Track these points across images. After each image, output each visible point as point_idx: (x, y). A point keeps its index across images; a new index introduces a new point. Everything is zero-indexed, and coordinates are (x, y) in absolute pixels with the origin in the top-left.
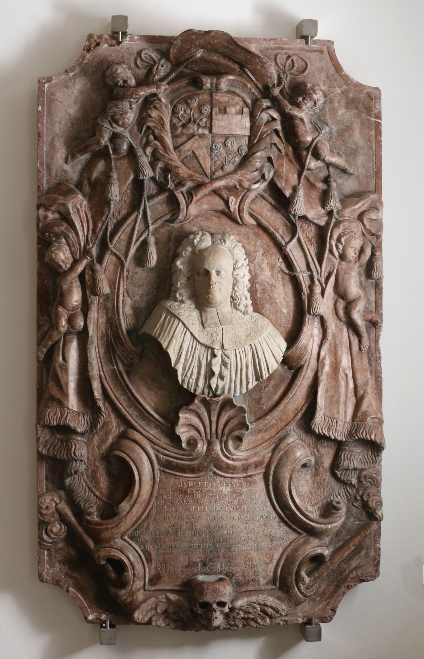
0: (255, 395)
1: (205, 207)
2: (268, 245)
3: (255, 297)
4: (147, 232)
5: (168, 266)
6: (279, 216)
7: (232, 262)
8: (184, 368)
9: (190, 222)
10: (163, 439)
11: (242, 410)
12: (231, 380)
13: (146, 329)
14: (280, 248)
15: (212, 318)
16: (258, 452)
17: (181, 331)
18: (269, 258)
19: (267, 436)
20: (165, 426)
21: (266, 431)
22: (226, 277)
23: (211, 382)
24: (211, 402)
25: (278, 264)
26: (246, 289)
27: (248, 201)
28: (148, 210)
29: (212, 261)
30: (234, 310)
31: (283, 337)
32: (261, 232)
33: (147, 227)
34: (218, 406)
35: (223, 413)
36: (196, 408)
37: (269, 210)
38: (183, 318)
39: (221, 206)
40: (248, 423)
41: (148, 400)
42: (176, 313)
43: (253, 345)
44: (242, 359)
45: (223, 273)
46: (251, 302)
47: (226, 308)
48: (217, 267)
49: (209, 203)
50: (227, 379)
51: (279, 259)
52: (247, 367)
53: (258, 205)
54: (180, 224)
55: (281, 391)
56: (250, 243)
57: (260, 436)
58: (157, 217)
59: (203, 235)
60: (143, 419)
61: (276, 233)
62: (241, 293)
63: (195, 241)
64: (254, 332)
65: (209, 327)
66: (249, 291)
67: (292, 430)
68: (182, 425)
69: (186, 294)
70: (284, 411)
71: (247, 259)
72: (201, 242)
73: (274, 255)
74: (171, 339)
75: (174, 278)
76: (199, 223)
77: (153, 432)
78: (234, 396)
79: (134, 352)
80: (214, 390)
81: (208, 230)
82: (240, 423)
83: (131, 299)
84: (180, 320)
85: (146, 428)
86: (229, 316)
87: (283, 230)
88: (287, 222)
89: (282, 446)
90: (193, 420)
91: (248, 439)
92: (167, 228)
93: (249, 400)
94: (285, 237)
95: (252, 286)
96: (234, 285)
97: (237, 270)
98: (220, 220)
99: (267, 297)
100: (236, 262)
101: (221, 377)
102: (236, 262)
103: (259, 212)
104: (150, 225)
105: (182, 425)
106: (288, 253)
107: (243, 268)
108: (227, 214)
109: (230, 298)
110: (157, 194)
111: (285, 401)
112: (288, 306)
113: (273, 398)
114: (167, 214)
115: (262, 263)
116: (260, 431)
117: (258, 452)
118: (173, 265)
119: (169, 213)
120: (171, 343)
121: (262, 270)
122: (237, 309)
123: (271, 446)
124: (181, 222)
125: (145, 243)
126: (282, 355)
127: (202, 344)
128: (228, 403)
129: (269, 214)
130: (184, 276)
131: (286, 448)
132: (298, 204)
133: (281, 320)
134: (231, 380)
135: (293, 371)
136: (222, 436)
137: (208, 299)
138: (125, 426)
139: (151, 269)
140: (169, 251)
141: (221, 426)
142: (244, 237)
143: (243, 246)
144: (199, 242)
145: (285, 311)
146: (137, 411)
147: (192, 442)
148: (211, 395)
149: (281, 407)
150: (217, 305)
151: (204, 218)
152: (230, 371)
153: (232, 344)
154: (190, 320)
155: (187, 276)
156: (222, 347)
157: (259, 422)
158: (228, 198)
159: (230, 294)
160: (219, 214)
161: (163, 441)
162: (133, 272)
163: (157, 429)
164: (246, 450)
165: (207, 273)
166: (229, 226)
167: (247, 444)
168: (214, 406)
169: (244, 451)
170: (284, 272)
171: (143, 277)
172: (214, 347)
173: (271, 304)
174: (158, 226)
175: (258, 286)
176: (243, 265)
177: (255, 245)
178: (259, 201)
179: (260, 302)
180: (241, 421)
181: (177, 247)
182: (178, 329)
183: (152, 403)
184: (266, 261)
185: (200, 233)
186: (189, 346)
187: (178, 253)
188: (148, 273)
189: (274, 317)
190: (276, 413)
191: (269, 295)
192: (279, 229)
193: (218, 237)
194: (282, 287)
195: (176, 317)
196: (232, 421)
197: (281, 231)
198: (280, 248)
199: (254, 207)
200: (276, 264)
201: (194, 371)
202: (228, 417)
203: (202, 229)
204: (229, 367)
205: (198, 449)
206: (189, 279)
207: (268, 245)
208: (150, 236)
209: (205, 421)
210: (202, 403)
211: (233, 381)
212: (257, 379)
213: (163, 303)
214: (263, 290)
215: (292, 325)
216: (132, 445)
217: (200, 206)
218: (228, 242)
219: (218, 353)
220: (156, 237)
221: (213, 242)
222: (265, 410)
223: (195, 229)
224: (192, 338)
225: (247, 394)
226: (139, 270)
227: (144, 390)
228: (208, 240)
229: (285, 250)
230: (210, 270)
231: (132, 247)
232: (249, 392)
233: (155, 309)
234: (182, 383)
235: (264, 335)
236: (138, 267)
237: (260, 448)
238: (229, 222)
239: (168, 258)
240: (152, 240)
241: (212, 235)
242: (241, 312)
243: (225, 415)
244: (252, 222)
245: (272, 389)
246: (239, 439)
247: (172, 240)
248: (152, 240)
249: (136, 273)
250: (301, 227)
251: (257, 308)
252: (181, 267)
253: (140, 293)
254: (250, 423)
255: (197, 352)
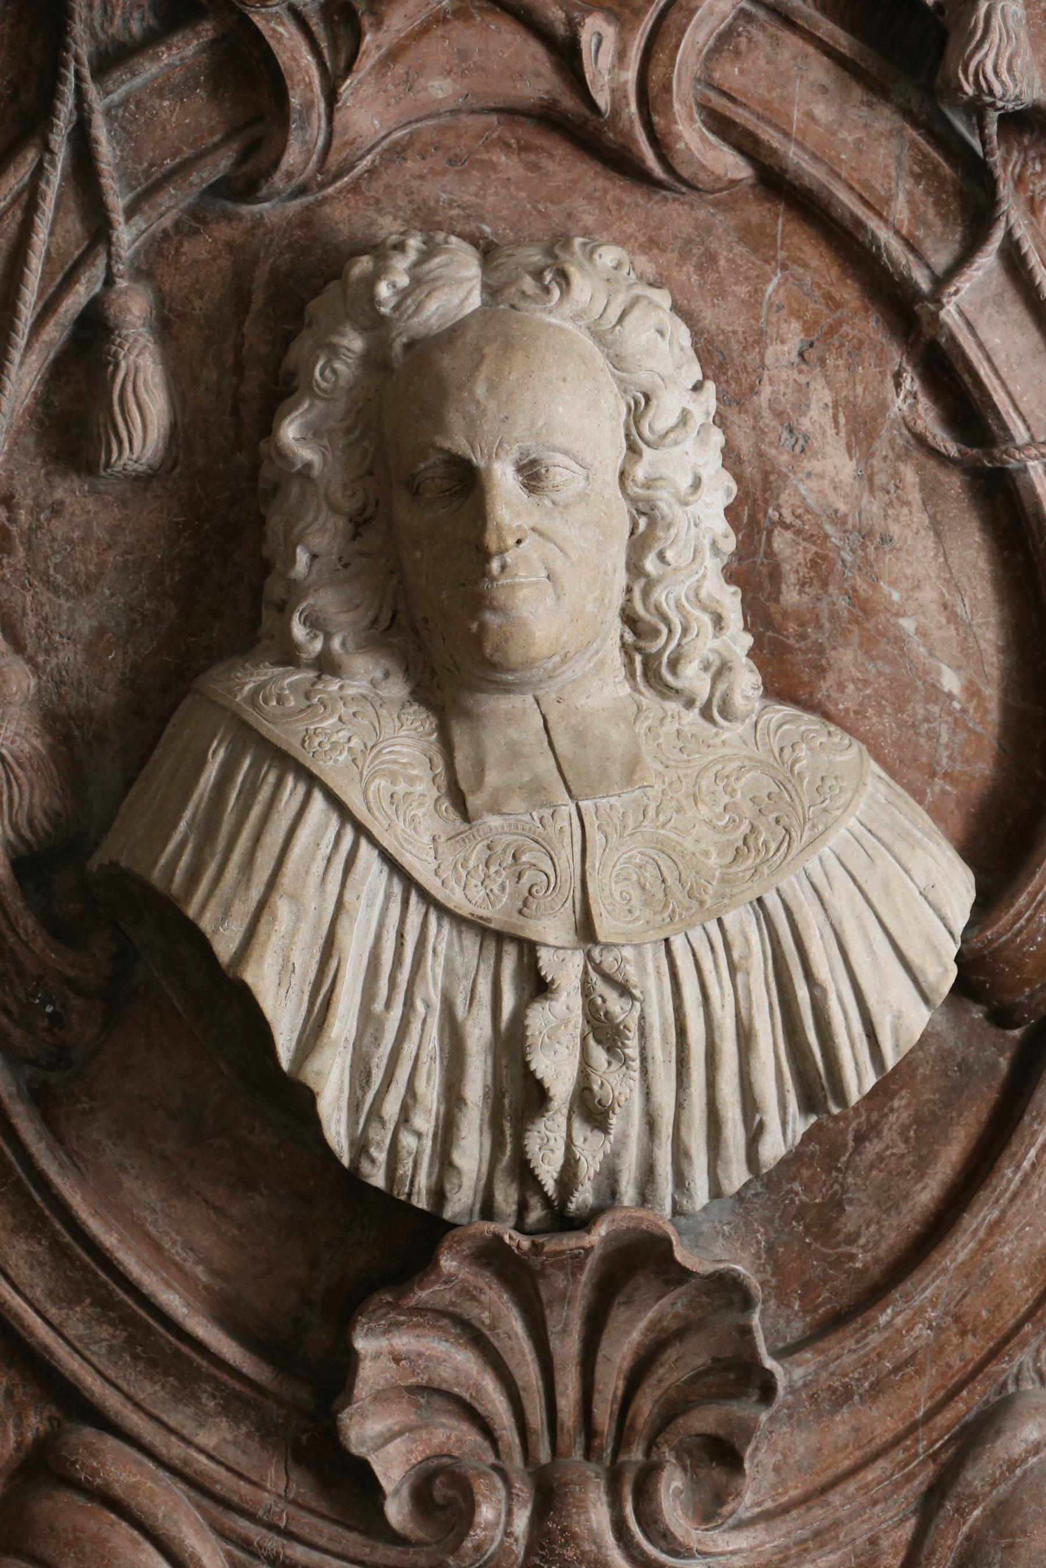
0: (799, 1198)
1: (440, 89)
2: (828, 297)
3: (773, 608)
4: (101, 262)
5: (242, 459)
6: (885, 119)
7: (613, 409)
8: (360, 1071)
9: (355, 188)
10: (274, 1477)
11: (727, 1289)
12: (651, 1124)
13: (116, 850)
14: (906, 312)
15: (514, 754)
16: (837, 1524)
17: (325, 850)
18: (844, 375)
19: (882, 1420)
20: (279, 1401)
21: (877, 1390)
22: (583, 497)
23: (533, 1144)
24: (536, 1262)
25: (899, 405)
26: (712, 566)
27: (696, 38)
28: (100, 131)
29: (492, 405)
30: (649, 698)
31: (952, 838)
32: (782, 224)
33: (99, 231)
34: (584, 1277)
35: (618, 1316)
36: (449, 1296)
37: (824, 90)
38: (331, 767)
39: (535, 79)
40: (769, 1363)
41: (171, 1261)
42: (286, 736)
43: (772, 901)
44: (714, 991)
45: (563, 474)
46: (748, 640)
47: (601, 687)
48: (520, 438)
49: (460, 65)
50: (627, 1122)
51: (897, 376)
52: (745, 1038)
53: (758, 61)
54: (295, 205)
55: (952, 1154)
56: (720, 292)
57: (842, 1424)
58: (157, 173)
59: (427, 254)
60: (152, 1364)
61: (873, 223)
62: (682, 591)
63: (384, 290)
64: (778, 822)
65: (495, 809)
66: (731, 576)
67: (1029, 1373)
68: (379, 1397)
69: (344, 618)
70: (979, 1272)
71: (710, 386)
72: (419, 295)
73: (869, 356)
74: (263, 904)
75: (275, 523)
76: (409, 193)
77: (213, 1439)
78: (677, 1211)
79: (68, 981)
80: (550, 1187)
81: (470, 227)
82: (719, 1365)
83: (37, 669)
84: (312, 780)
85: (172, 1421)
86: (617, 735)
87: (911, 202)
88: (935, 155)
89: (977, 1475)
90: (440, 1361)
91: (773, 1449)
92: (224, 232)
93: (768, 1221)
94: (928, 246)
95: (745, 551)
96: (638, 546)
97: (647, 453)
98: (536, 167)
99: (842, 603)
100: (640, 406)
101: (591, 1110)
102: (640, 406)
103: (766, 104)
104: (118, 217)
105: (379, 1397)
106: (952, 338)
107: (689, 442)
108: (574, 127)
109: (616, 628)
110: (153, 39)
111: (981, 1216)
112: (966, 655)
113: (906, 1196)
114: (216, 147)
115: (802, 407)
116: (843, 1396)
117: (837, 1524)
118: (263, 446)
119: (227, 139)
120: (262, 928)
121: (804, 446)
122: (665, 691)
123: (909, 1478)
124: (302, 190)
125: (94, 332)
126: (954, 951)
127: (460, 921)
128: (642, 1259)
129: (821, 111)
130: (335, 510)
131: (1003, 1488)
132: (994, 36)
133: (933, 736)
134: (651, 1124)
135: (1017, 1033)
136: (622, 1440)
137: (478, 640)
138: (53, 1410)
139: (144, 480)
140: (239, 368)
141: (611, 1382)
142: (684, 256)
143: (677, 308)
144: (403, 294)
145: (951, 682)
146: (112, 1323)
147: (440, 1491)
148: (536, 1214)
149: (961, 1248)
150: (536, 673)
151: (437, 161)
152: (644, 1071)
153: (646, 903)
154: (374, 775)
155: (348, 505)
156: (586, 930)
157: (831, 1343)
158: (573, 26)
159: (618, 599)
160: (527, 132)
161: (275, 1485)
162: (37, 508)
163: (236, 1421)
164: (767, 1516)
165: (467, 482)
166: (589, 198)
167: (771, 1476)
168: (560, 1281)
169: (752, 1522)
170: (933, 452)
171: (98, 532)
172: (533, 930)
173: (868, 643)
174: (167, 222)
175: (782, 542)
176: (685, 418)
177: (753, 303)
178: (760, 37)
179: (802, 637)
180: (727, 1353)
181: (286, 340)
182: (303, 835)
183: (199, 1271)
184: (821, 394)
185: (414, 243)
186: (378, 938)
187: (293, 374)
188: (124, 503)
189: (888, 722)
190: (934, 1286)
191: (853, 594)
192: (888, 200)
193: (524, 263)
194: (930, 542)
195: (288, 763)
196: (671, 1354)
197: (900, 210)
198: (906, 312)
199: (729, 73)
200: (883, 407)
201: (421, 1085)
202: (649, 1329)
203: (429, 222)
204: (632, 1049)
205: (478, 1534)
206: (359, 524)
207: (828, 297)
208: (122, 284)
209: (512, 1364)
210: (487, 1265)
211: (666, 1129)
212: (810, 1103)
213: (213, 683)
214: (814, 564)
215: (999, 762)
216: (92, 1525)
217: (408, 84)
218: (583, 288)
219: (565, 968)
220: (158, 291)
221: (492, 292)
222: (866, 1269)
223: (388, 227)
224: (397, 888)
225: (758, 1187)
226: (68, 490)
227: (144, 1194)
228: (460, 282)
229: (935, 317)
230: (479, 461)
231: (16, 355)
232: (768, 1182)
233: (174, 720)
234: (355, 1160)
235: (838, 837)
236: (64, 475)
237: (851, 1499)
238: (590, 176)
239: (235, 411)
240: (135, 308)
241: (488, 252)
242: (690, 704)
243: (632, 1322)
244: (729, 164)
245: (901, 1148)
246: (723, 1454)
247: (258, 300)
248: (135, 308)
249: (57, 510)
250: (1019, 182)
251: (788, 673)
252: (306, 453)
253: (85, 625)
254: (778, 1355)
255: (434, 970)
